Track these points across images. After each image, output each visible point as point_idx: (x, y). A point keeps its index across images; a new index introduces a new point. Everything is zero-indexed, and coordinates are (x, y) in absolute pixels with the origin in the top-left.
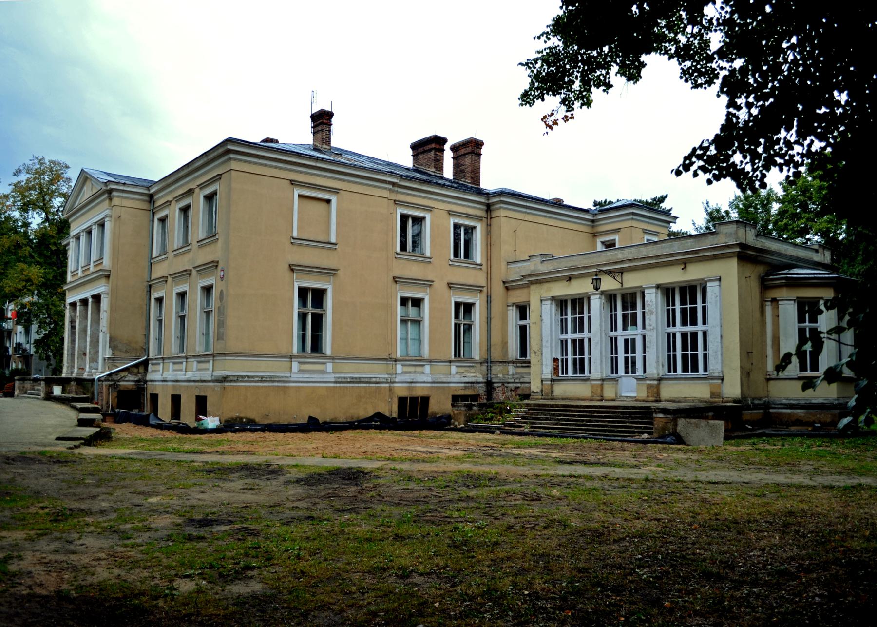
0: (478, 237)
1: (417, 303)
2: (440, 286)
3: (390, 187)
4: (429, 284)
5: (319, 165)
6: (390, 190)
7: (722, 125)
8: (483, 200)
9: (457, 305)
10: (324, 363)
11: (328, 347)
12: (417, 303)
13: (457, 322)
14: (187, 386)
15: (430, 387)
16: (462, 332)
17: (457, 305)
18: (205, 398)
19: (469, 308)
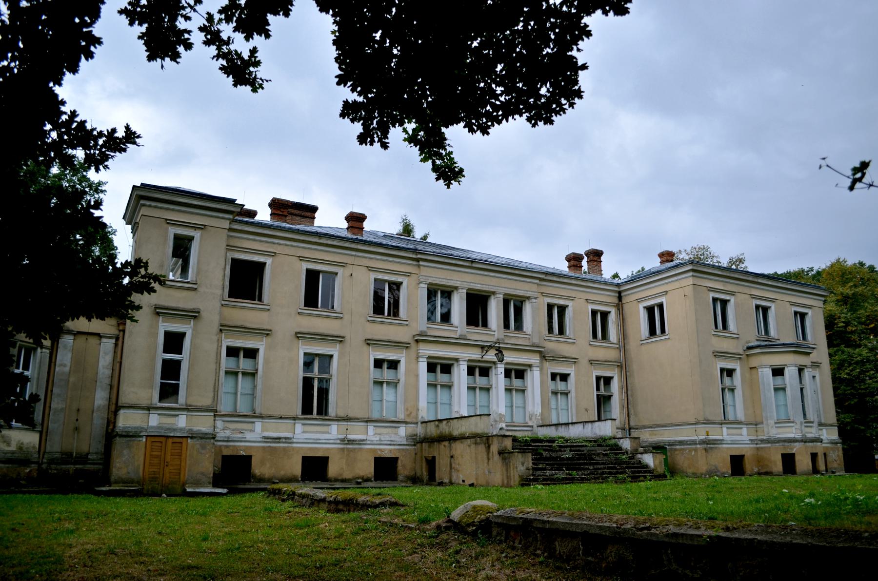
0: (612, 318)
1: (394, 365)
2: (584, 362)
3: (538, 281)
4: (339, 339)
5: (322, 241)
6: (538, 284)
7: (337, 59)
8: (617, 289)
9: (598, 379)
10: (253, 422)
11: (332, 411)
12: (564, 377)
13: (309, 375)
14: (263, 447)
15: (399, 449)
16: (603, 401)
17: (598, 379)
18: (792, 456)
19: (608, 380)
